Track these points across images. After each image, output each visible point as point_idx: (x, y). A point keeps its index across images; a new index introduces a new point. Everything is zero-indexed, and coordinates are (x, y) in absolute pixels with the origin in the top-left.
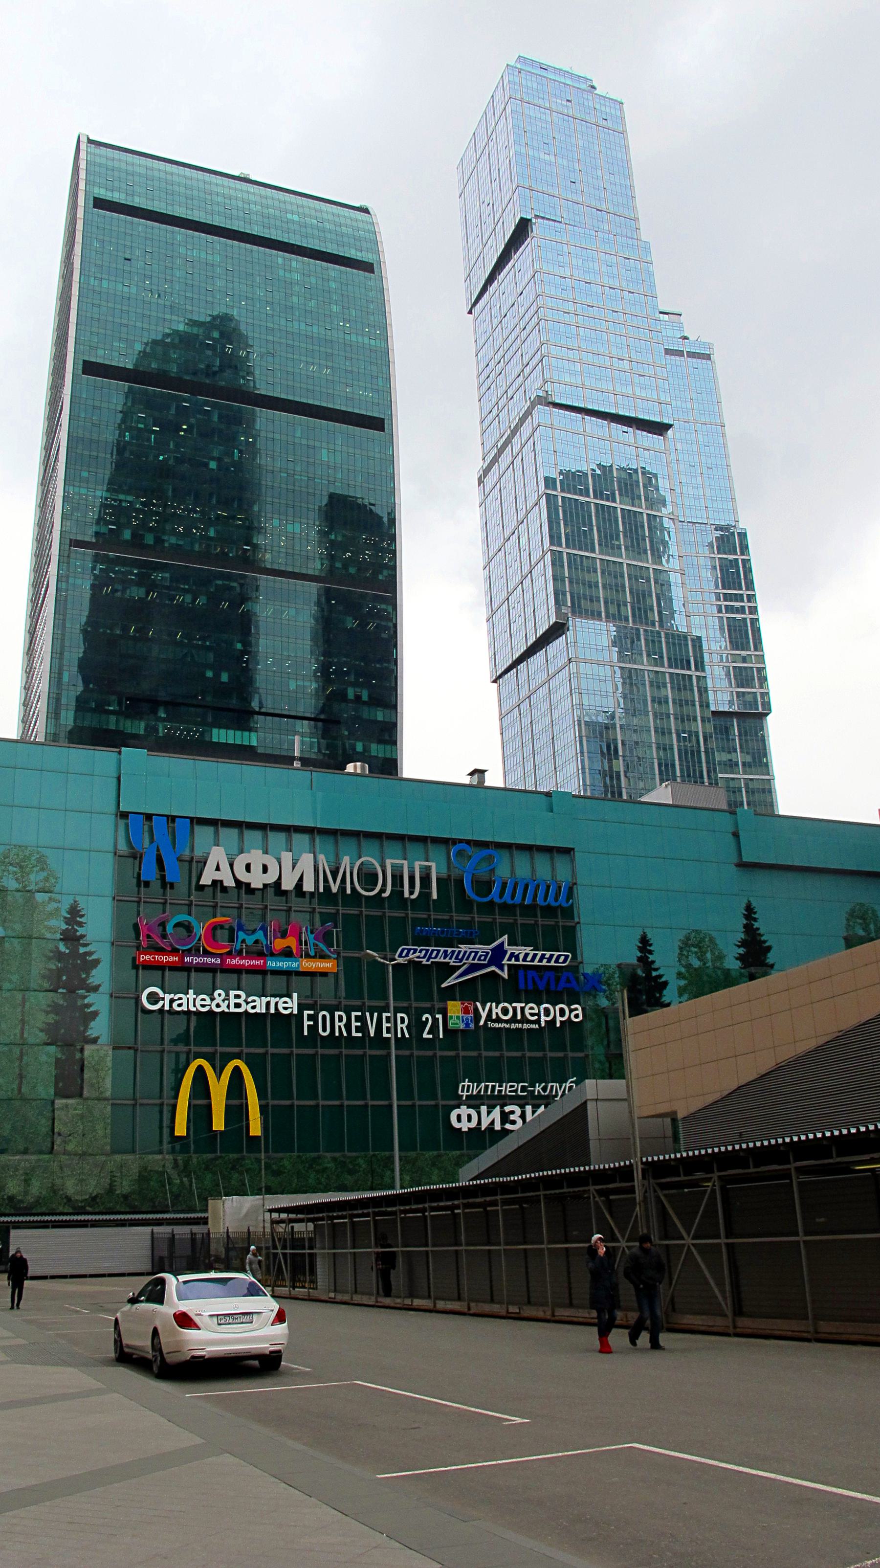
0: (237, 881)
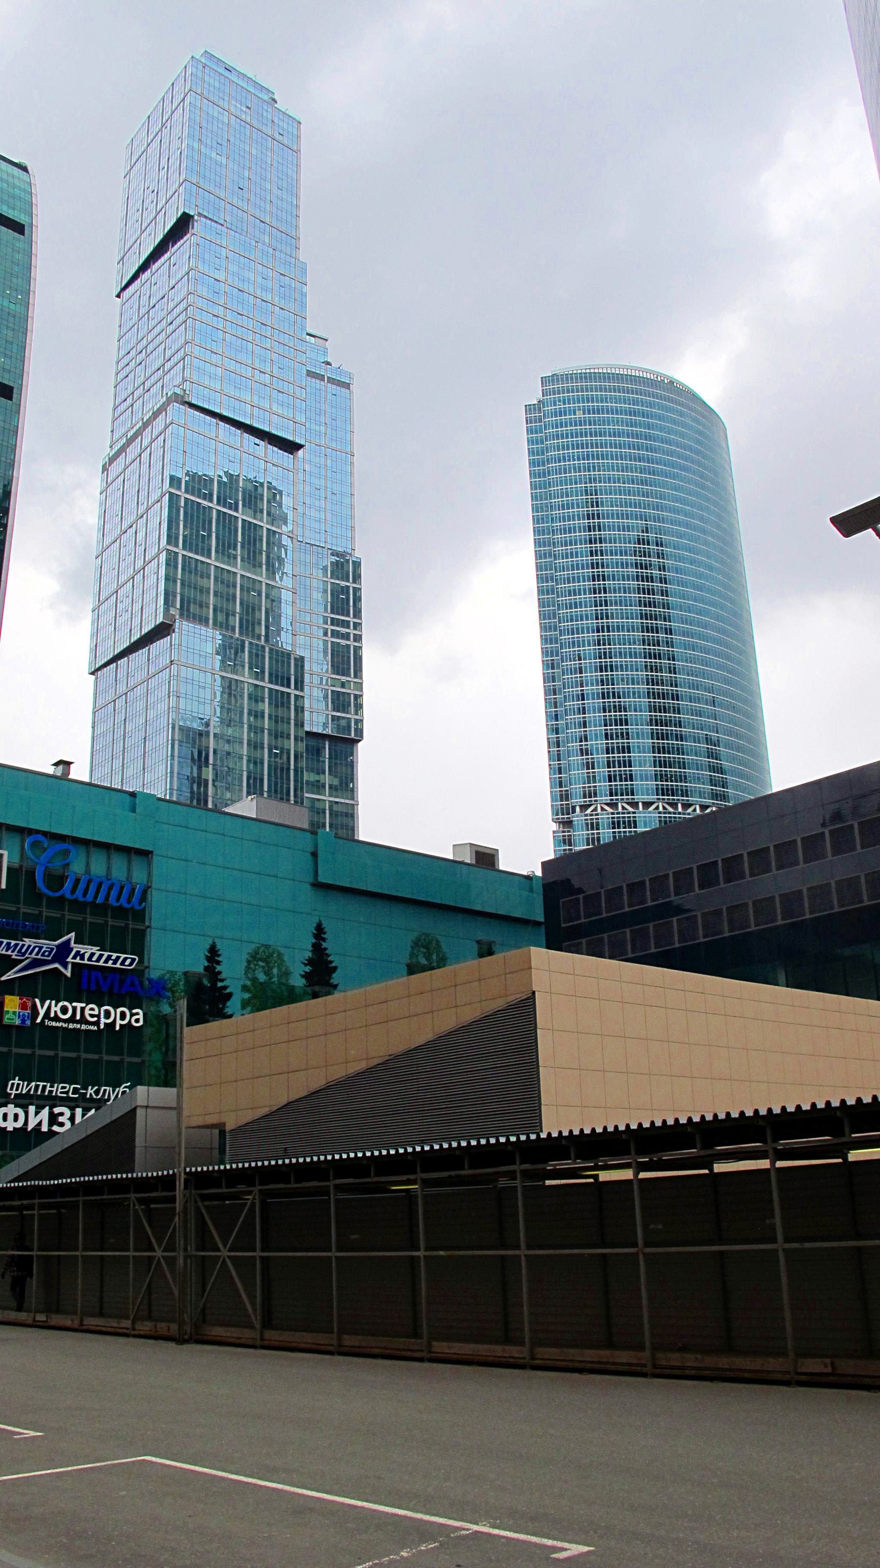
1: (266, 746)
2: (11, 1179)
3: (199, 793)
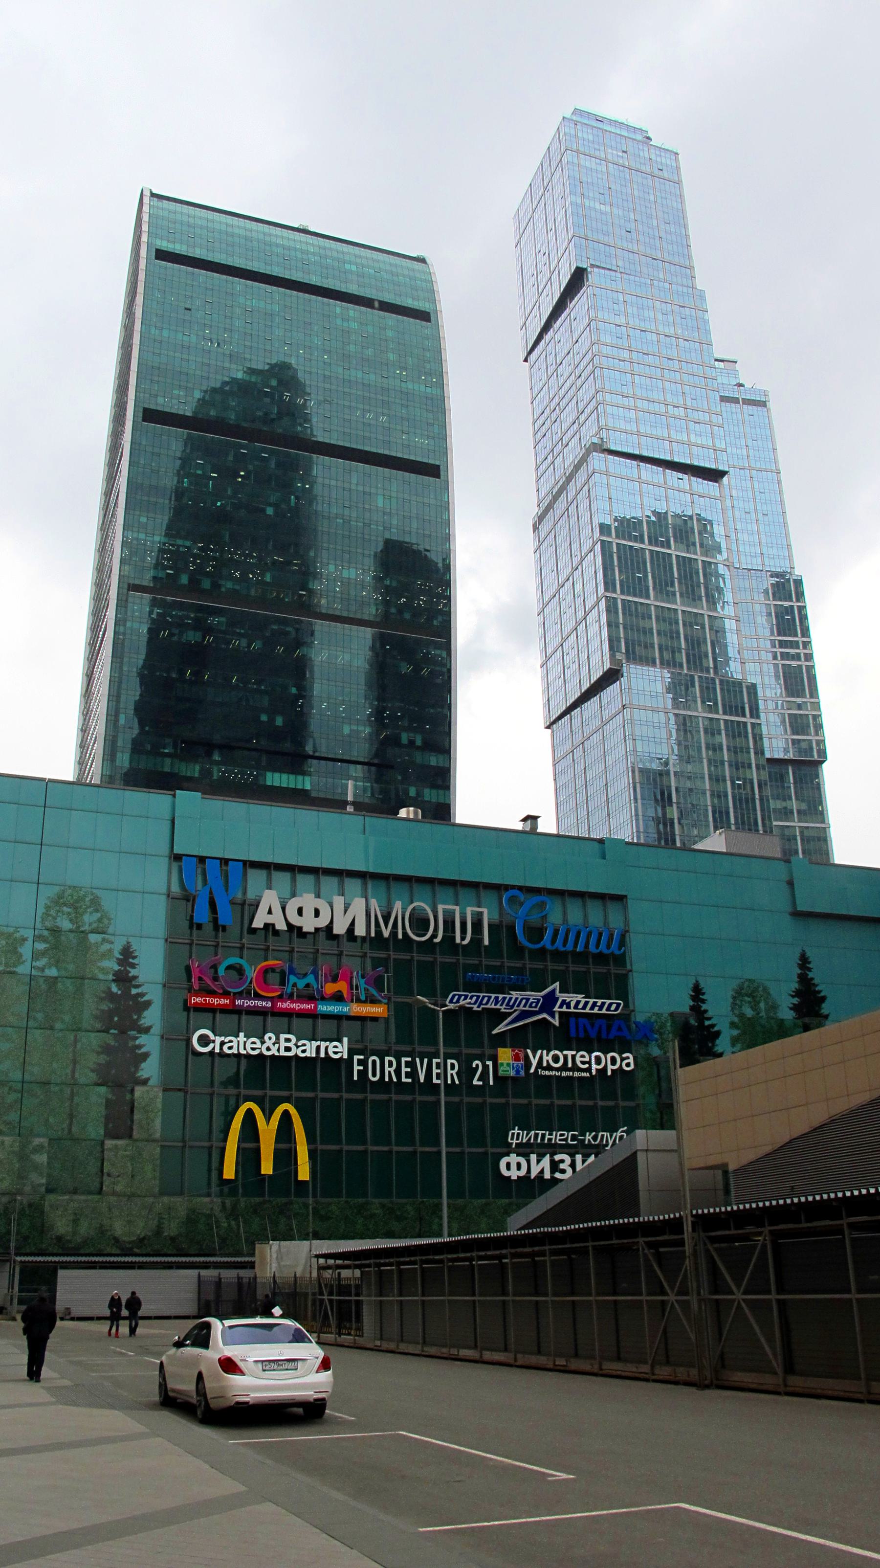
0: (289, 924)
1: (728, 778)
2: (519, 1227)
3: (666, 833)
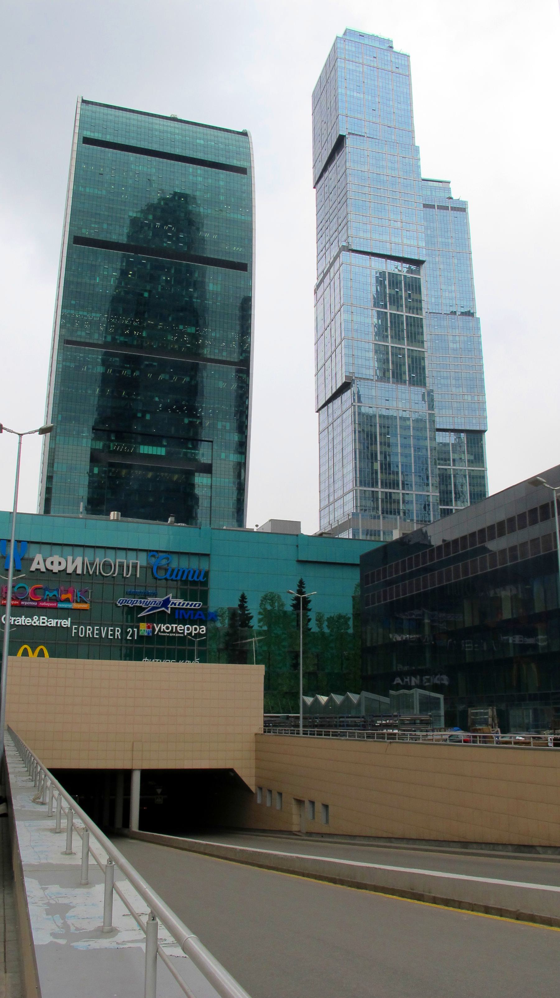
0: (47, 569)
